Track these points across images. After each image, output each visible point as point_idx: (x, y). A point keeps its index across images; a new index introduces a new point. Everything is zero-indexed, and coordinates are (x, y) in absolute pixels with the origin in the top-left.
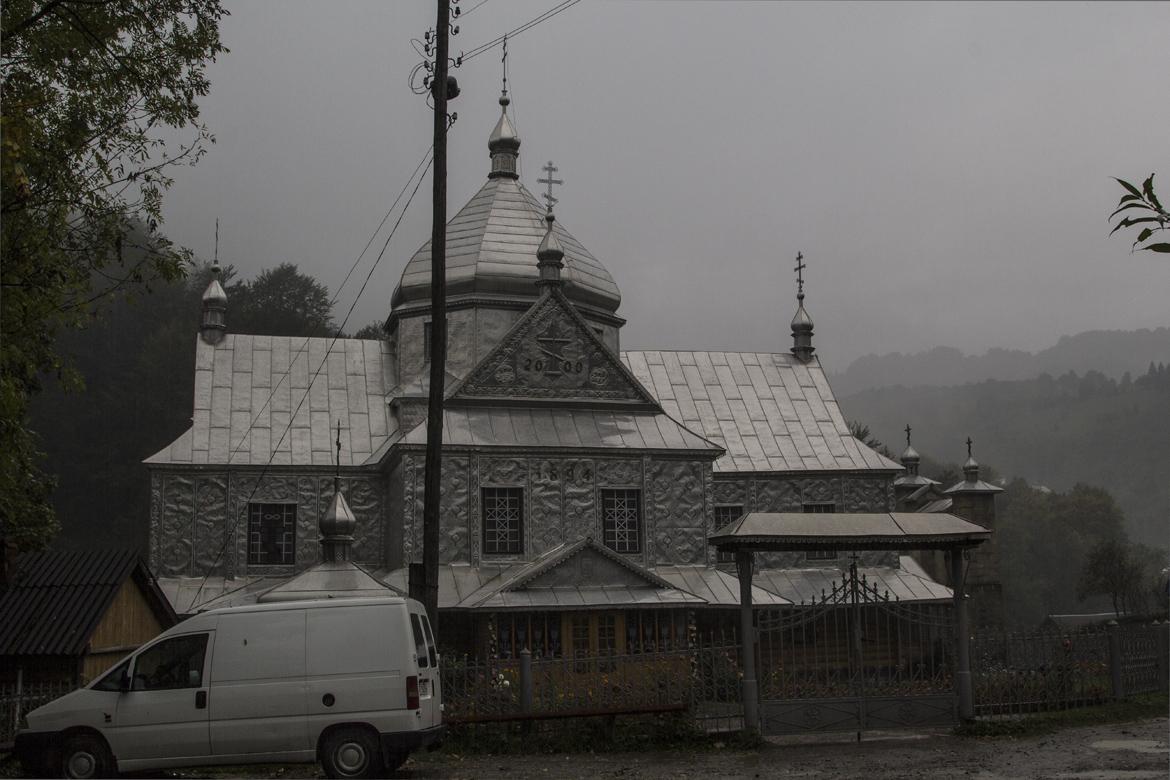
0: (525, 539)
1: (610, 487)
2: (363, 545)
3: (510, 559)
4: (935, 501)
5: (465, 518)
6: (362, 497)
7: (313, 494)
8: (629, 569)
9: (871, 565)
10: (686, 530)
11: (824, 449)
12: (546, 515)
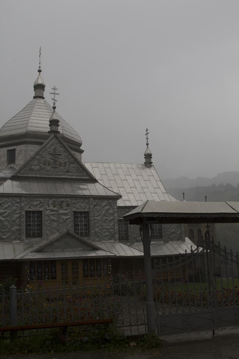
0: (43, 231)
1: (77, 210)
3: (37, 239)
8: (82, 241)
9: (175, 240)
10: (107, 227)
12: (51, 221)
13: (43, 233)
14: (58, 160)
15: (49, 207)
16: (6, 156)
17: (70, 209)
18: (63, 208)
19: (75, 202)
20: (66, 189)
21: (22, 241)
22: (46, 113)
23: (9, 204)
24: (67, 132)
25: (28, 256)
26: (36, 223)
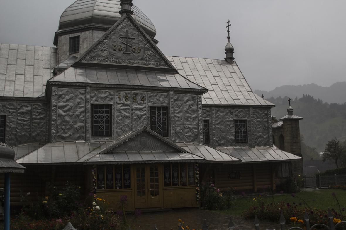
0: (113, 129)
1: (154, 105)
2: (38, 134)
3: (105, 139)
4: (274, 123)
5: (83, 118)
6: (38, 112)
7: (14, 111)
8: (165, 142)
9: (262, 145)
10: (190, 126)
11: (242, 96)
12: (123, 118)
13: (113, 132)
14: (132, 45)
15: (120, 100)
16: (69, 44)
17: (145, 103)
18: (137, 102)
19: (152, 95)
20: (142, 80)
21: (87, 141)
22: (115, 6)
23: (72, 95)
24: (140, 18)
25: (95, 158)
26: (104, 119)
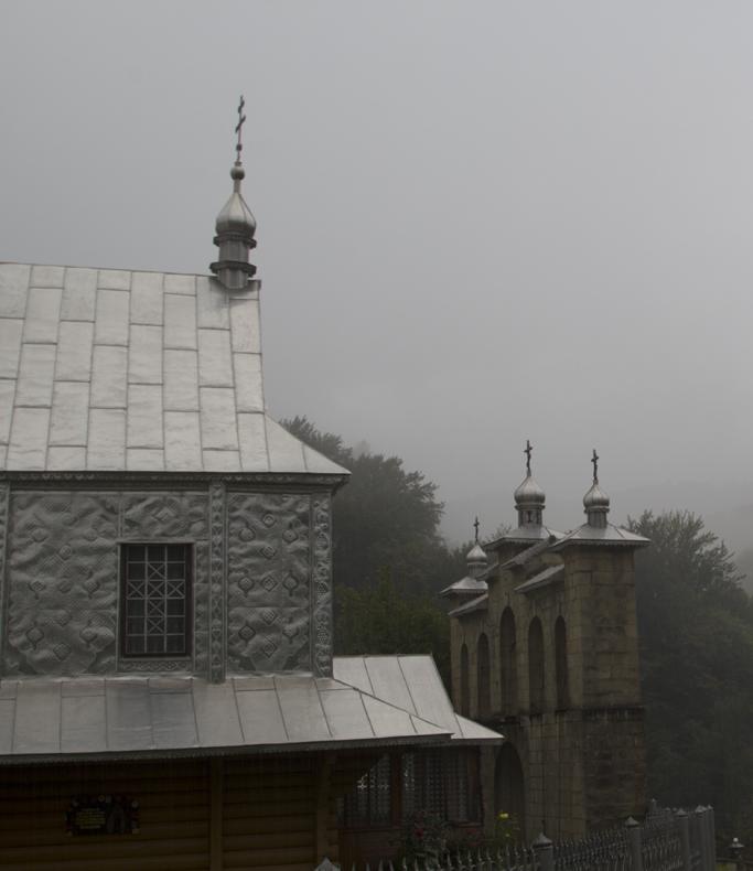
9: (270, 670)
